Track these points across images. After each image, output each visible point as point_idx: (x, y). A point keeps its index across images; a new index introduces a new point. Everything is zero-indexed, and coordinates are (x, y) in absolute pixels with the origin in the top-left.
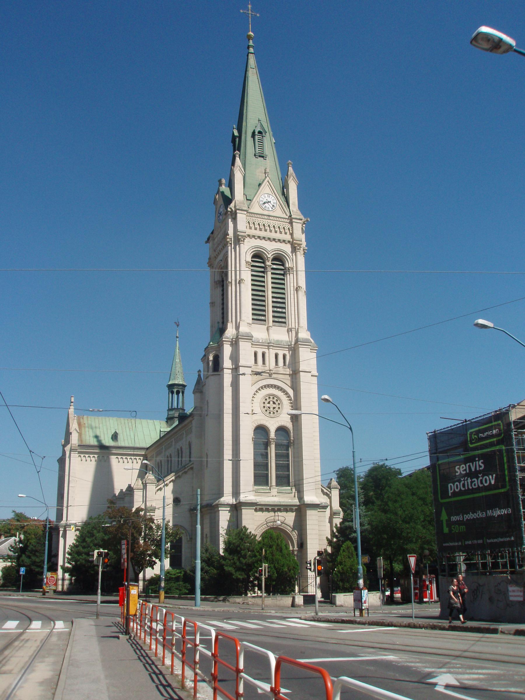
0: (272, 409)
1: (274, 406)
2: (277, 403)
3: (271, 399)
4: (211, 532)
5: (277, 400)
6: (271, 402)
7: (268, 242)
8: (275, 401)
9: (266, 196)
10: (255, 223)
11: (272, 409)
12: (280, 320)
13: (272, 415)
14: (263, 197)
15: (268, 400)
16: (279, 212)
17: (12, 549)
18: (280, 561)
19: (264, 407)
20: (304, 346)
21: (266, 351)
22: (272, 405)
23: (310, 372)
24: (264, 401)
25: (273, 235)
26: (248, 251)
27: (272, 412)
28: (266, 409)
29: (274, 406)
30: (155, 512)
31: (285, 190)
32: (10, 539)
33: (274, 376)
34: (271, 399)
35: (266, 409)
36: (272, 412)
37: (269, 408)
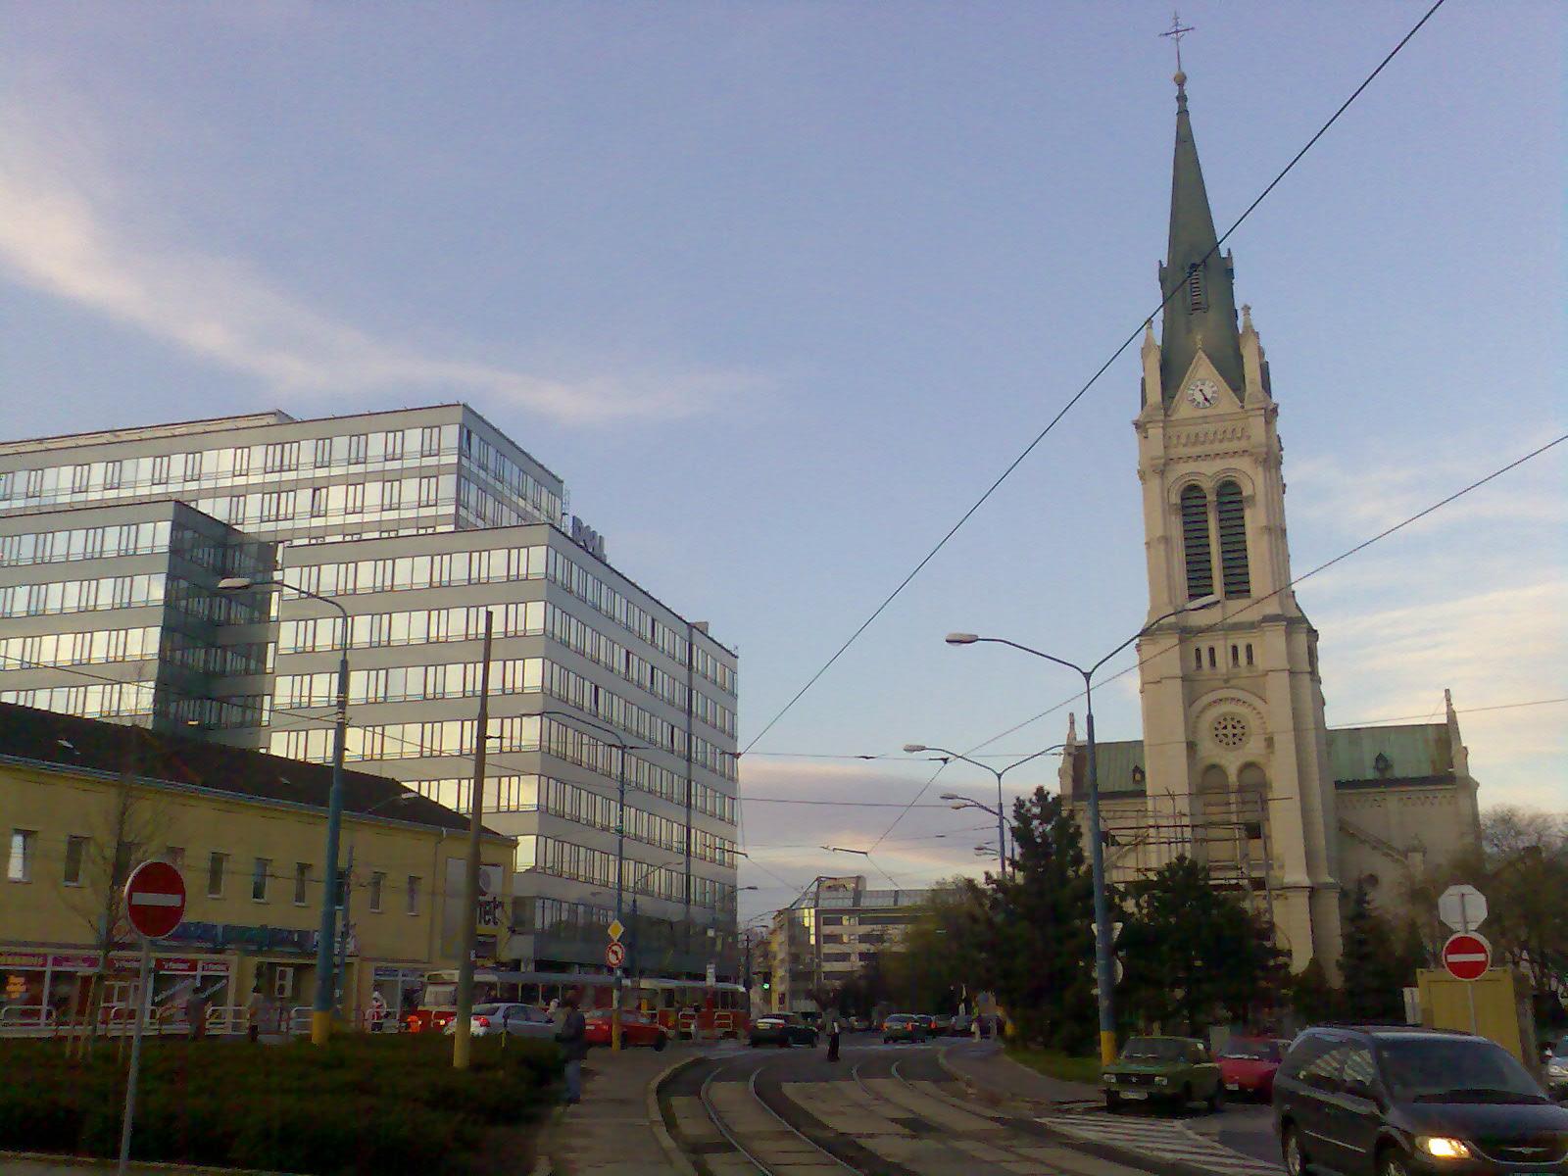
15: (1223, 724)
25: (1218, 447)
37: (1225, 728)
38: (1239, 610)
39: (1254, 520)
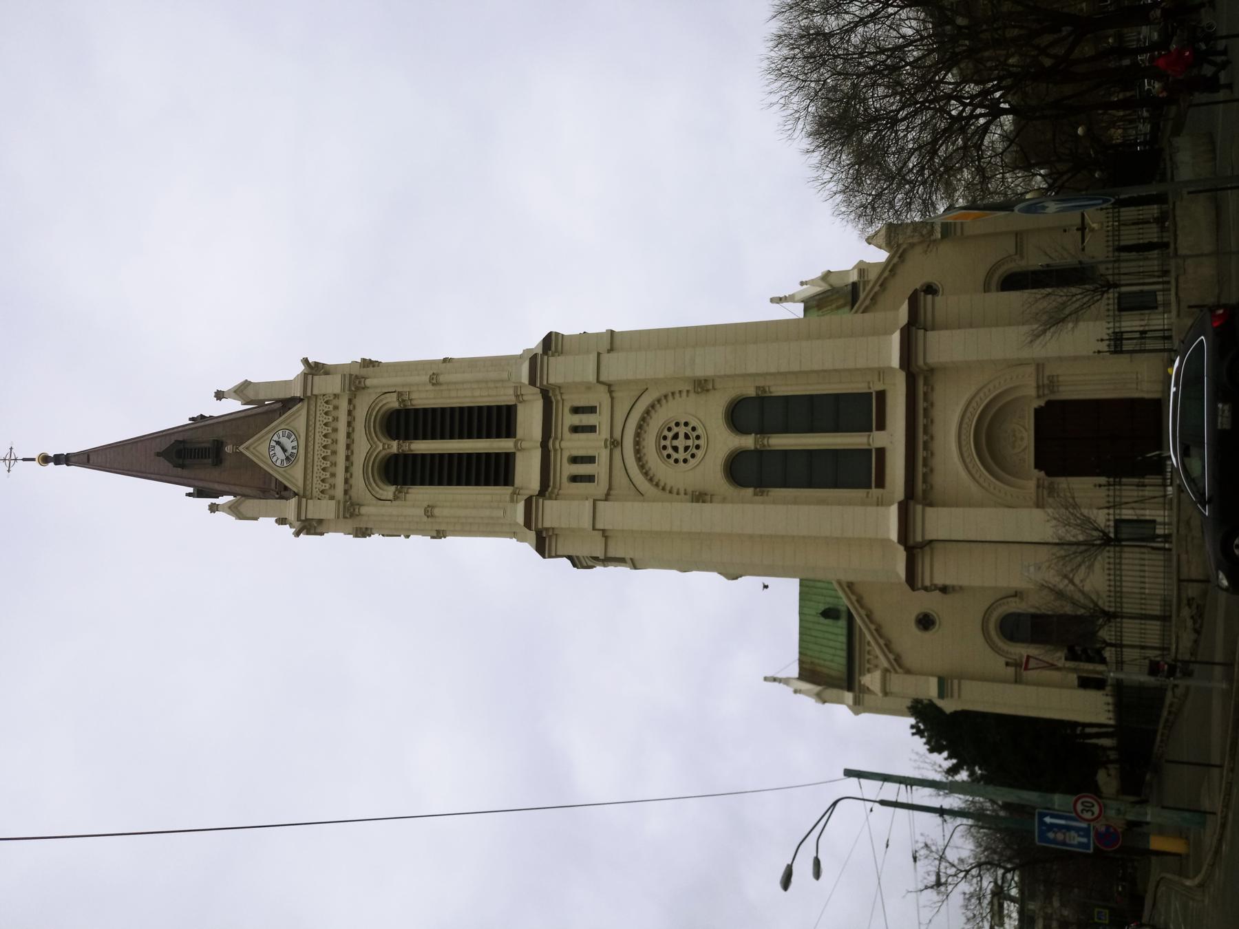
0: (689, 443)
1: (681, 436)
2: (675, 430)
3: (667, 443)
4: (894, 257)
5: (670, 429)
6: (675, 443)
7: (355, 447)
8: (670, 435)
9: (273, 452)
10: (323, 477)
11: (689, 443)
12: (465, 464)
13: (701, 442)
14: (279, 462)
15: (670, 451)
16: (300, 423)
17: (855, 39)
18: (1035, 332)
19: (685, 461)
20: (545, 372)
21: (566, 455)
22: (680, 443)
23: (599, 354)
24: (672, 461)
26: (373, 493)
27: (697, 442)
28: (695, 434)
29: (681, 436)
30: (864, 269)
31: (266, 403)
32: (860, 629)
33: (617, 435)
34: (667, 443)
35: (695, 434)
36: (697, 442)
38: (530, 420)
39: (425, 399)
